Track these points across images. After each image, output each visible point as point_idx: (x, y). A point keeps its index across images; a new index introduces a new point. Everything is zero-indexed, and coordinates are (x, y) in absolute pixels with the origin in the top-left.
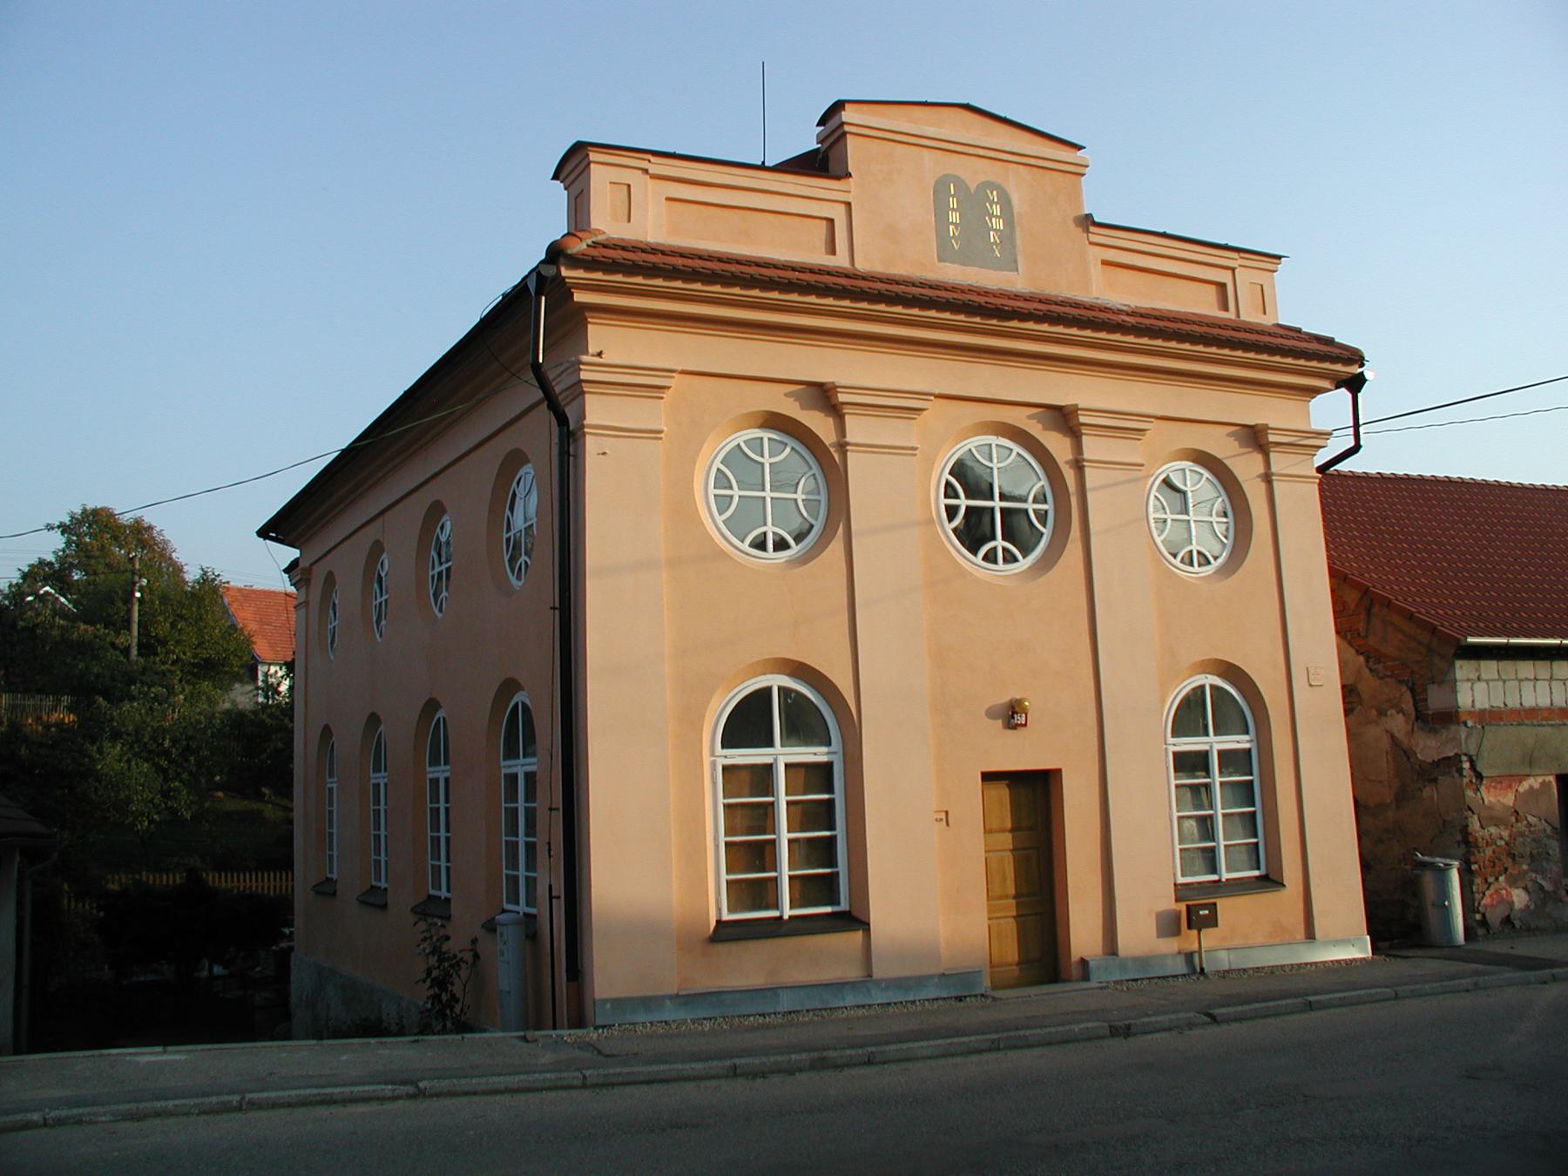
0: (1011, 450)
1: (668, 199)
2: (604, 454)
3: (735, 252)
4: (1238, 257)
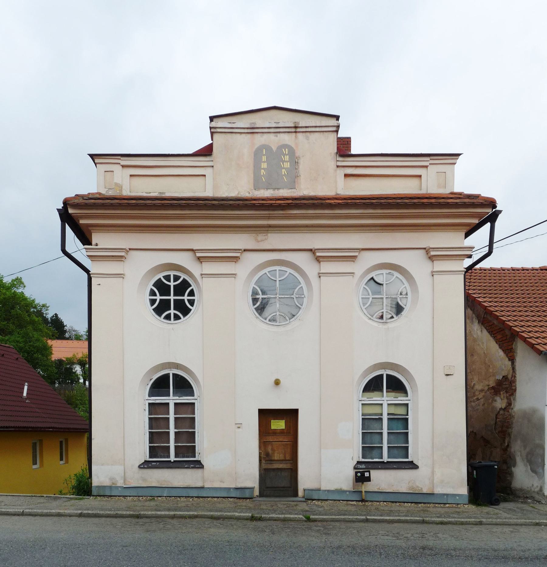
0: (383, 274)
1: (131, 176)
2: (99, 284)
3: (358, 194)
4: (429, 160)
